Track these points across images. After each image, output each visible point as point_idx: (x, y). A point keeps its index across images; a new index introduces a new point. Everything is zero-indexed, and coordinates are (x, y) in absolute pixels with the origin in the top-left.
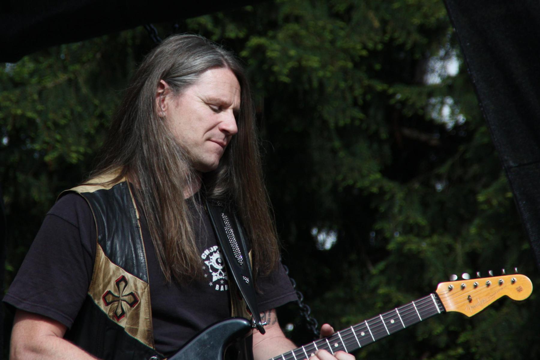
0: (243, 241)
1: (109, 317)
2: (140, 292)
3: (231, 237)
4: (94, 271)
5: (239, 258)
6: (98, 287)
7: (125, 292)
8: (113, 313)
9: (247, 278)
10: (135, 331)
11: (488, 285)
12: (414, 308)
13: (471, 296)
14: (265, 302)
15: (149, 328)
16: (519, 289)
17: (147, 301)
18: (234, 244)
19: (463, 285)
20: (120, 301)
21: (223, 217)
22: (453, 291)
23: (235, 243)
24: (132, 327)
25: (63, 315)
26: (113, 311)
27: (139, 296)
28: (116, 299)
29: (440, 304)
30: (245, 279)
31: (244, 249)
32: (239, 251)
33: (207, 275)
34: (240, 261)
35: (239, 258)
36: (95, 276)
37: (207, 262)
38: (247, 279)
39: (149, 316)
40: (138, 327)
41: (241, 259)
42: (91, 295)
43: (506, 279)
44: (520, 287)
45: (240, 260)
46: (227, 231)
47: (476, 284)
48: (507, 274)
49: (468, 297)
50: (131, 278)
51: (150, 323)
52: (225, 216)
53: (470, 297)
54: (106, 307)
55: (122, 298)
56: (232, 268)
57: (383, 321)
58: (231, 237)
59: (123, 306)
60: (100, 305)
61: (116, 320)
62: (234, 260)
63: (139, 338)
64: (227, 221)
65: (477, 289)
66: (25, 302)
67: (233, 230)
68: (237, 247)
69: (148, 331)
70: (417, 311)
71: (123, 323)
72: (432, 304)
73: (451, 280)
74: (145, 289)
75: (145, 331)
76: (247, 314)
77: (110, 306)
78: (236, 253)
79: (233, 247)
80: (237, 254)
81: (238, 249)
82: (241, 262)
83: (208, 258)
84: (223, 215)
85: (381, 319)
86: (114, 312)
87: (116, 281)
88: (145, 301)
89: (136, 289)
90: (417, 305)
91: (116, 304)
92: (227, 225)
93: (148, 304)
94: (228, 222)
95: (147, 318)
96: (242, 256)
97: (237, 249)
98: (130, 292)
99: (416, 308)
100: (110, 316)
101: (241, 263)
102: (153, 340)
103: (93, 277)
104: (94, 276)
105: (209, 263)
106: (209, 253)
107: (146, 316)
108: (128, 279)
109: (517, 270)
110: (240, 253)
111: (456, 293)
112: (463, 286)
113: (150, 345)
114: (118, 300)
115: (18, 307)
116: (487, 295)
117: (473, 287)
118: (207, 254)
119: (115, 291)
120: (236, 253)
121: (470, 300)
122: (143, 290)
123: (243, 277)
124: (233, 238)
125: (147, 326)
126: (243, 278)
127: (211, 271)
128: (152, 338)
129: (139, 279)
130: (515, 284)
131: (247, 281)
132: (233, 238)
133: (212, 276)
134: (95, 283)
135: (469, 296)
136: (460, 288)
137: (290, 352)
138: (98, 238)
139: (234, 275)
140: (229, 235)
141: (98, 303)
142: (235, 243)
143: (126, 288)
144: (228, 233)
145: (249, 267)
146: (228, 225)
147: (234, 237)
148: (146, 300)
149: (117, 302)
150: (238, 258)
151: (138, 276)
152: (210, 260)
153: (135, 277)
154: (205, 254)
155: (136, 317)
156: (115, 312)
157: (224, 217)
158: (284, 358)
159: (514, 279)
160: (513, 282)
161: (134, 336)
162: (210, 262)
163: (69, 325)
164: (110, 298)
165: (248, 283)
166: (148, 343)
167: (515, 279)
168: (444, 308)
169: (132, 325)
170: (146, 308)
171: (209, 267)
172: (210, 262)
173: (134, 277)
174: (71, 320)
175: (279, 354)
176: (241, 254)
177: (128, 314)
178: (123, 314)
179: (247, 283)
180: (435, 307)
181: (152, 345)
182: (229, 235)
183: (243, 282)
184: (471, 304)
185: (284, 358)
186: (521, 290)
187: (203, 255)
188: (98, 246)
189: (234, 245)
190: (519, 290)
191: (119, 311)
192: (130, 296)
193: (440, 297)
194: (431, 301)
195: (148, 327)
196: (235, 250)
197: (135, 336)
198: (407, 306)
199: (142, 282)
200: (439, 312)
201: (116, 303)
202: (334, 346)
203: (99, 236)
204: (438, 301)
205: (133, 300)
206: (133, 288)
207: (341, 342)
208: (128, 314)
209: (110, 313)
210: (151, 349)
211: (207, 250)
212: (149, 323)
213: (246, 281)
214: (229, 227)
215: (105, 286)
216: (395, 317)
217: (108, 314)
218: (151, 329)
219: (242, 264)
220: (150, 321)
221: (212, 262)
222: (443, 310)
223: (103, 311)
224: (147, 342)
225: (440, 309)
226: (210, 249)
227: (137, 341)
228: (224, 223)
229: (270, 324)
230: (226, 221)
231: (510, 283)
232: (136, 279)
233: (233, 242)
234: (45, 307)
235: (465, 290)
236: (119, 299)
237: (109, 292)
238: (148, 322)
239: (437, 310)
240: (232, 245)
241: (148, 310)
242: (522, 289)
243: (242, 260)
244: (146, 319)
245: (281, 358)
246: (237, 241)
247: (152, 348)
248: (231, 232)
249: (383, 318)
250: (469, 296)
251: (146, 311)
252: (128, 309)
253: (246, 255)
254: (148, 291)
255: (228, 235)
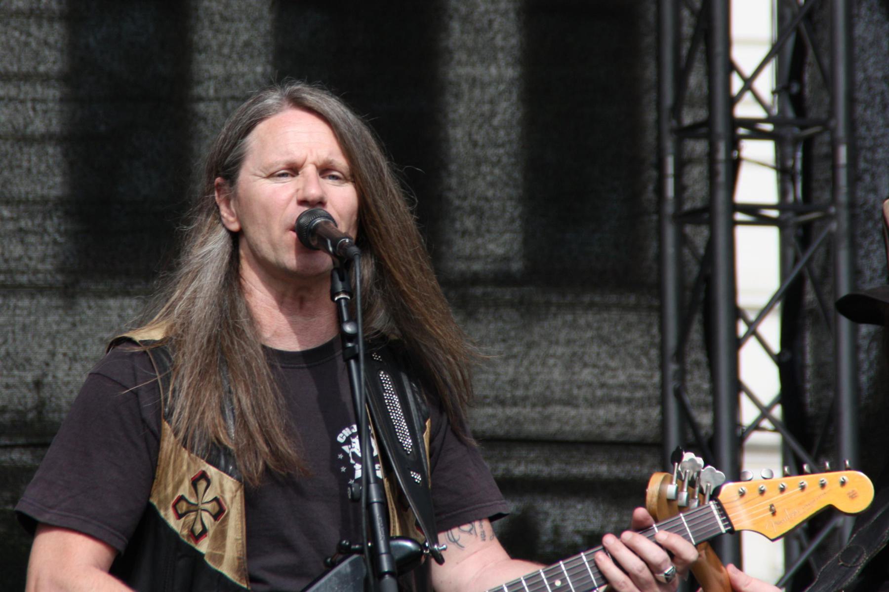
0: (415, 415)
1: (181, 537)
2: (228, 496)
3: (394, 409)
4: (158, 464)
5: (406, 443)
6: (165, 488)
7: (207, 496)
8: (188, 531)
9: (417, 475)
10: (220, 559)
11: (803, 488)
12: (683, 524)
13: (775, 505)
14: (459, 511)
15: (240, 555)
16: (851, 495)
17: (240, 512)
18: (398, 420)
19: (762, 487)
20: (199, 511)
21: (382, 376)
22: (746, 497)
23: (400, 418)
24: (215, 552)
25: (112, 530)
26: (188, 528)
27: (225, 503)
28: (192, 508)
29: (725, 518)
30: (414, 475)
31: (416, 428)
32: (407, 431)
33: (345, 469)
34: (407, 447)
35: (406, 443)
36: (160, 472)
37: (346, 448)
38: (418, 476)
39: (242, 535)
40: (224, 552)
41: (409, 445)
42: (155, 503)
43: (832, 478)
44: (853, 491)
45: (407, 446)
46: (387, 399)
47: (782, 487)
48: (832, 470)
49: (769, 507)
50: (215, 474)
51: (243, 547)
52: (386, 375)
53: (773, 507)
54: (178, 521)
55: (203, 507)
56: (393, 459)
57: (587, 564)
58: (394, 409)
59: (204, 519)
60: (168, 518)
61: (193, 542)
62: (397, 446)
63: (227, 569)
64: (388, 383)
65: (785, 494)
66: (51, 511)
67: (399, 398)
68: (403, 425)
69: (239, 559)
70: (688, 529)
71: (204, 547)
72: (585, 570)
73: (743, 478)
74: (236, 491)
75: (234, 558)
76: (416, 534)
77: (183, 519)
78: (401, 435)
79: (396, 425)
80: (402, 436)
81: (404, 428)
82: (409, 448)
83: (348, 442)
84: (382, 374)
85: (583, 560)
86: (190, 530)
87: (192, 479)
88: (236, 510)
89: (222, 491)
90: (688, 520)
91: (192, 516)
92: (389, 390)
93: (240, 515)
94: (389, 385)
95: (239, 537)
96: (412, 438)
97: (402, 429)
98: (214, 497)
99: (686, 524)
100: (183, 536)
101: (409, 451)
102: (246, 573)
103: (157, 474)
104: (159, 472)
105: (350, 449)
106: (350, 433)
107: (237, 536)
108: (212, 476)
109: (849, 463)
110: (408, 434)
111: (751, 500)
112: (762, 489)
113: (243, 581)
114: (195, 509)
115: (40, 519)
116: (800, 504)
117: (778, 491)
118: (347, 435)
119: (191, 494)
120: (401, 435)
121: (774, 514)
122: (233, 493)
123: (412, 473)
124: (397, 410)
125: (238, 552)
126: (411, 475)
127: (352, 461)
128: (245, 570)
129: (227, 476)
130: (847, 486)
131: (418, 480)
132: (397, 410)
133: (354, 470)
134: (159, 484)
135: (772, 506)
136: (757, 493)
137: (538, 573)
138: (164, 411)
139: (395, 469)
140: (390, 406)
141: (166, 515)
142: (400, 418)
143: (208, 491)
144: (388, 402)
145: (423, 456)
146: (390, 390)
147: (398, 410)
148: (237, 509)
149: (194, 513)
150: (404, 443)
151: (226, 471)
152: (351, 445)
153: (222, 473)
154: (344, 435)
155: (221, 535)
156: (191, 528)
157: (384, 378)
158: (506, 589)
159: (843, 479)
160: (843, 483)
161: (217, 566)
162: (352, 447)
163: (121, 546)
164: (183, 507)
165: (419, 482)
166: (239, 579)
167: (845, 478)
168: (731, 524)
169: (214, 549)
170: (237, 523)
171: (350, 455)
172: (352, 447)
173: (219, 472)
174: (125, 539)
175: (500, 585)
176: (410, 435)
177: (211, 532)
178: (204, 531)
179: (417, 482)
180: (717, 522)
181: (245, 582)
182: (390, 406)
183: (410, 481)
184: (776, 519)
185: (506, 589)
186: (856, 497)
187: (340, 437)
188: (164, 425)
189: (398, 422)
190: (853, 496)
191: (198, 528)
192: (214, 503)
193: (725, 506)
194: (680, 524)
195: (239, 552)
196: (400, 429)
197: (219, 567)
198: (672, 521)
199: (233, 481)
200: (723, 530)
201: (193, 515)
202: (555, 586)
203: (166, 408)
204: (722, 513)
205: (217, 509)
206: (219, 491)
207: (565, 578)
208: (211, 532)
209: (184, 531)
210: (243, 588)
211: (347, 429)
212: (241, 546)
213: (416, 478)
214: (391, 393)
215: (177, 487)
216: (560, 575)
217: (181, 532)
218: (243, 556)
219: (411, 452)
220: (242, 543)
221: (354, 448)
222: (729, 528)
223: (172, 527)
224: (237, 577)
225: (726, 526)
226: (353, 428)
227: (221, 576)
228: (383, 387)
229: (486, 540)
230: (386, 384)
231: (838, 485)
232: (221, 475)
233: (397, 417)
234: (83, 517)
235: (766, 495)
236: (198, 508)
237: (182, 498)
238: (240, 544)
239: (719, 528)
240: (395, 422)
241: (240, 526)
242: (856, 495)
243: (411, 446)
244: (237, 540)
245: (502, 589)
246: (404, 415)
247: (245, 586)
248: (395, 401)
249: (587, 559)
250: (772, 506)
251: (237, 527)
252: (211, 524)
253: (418, 437)
254: (241, 496)
255: (389, 405)
